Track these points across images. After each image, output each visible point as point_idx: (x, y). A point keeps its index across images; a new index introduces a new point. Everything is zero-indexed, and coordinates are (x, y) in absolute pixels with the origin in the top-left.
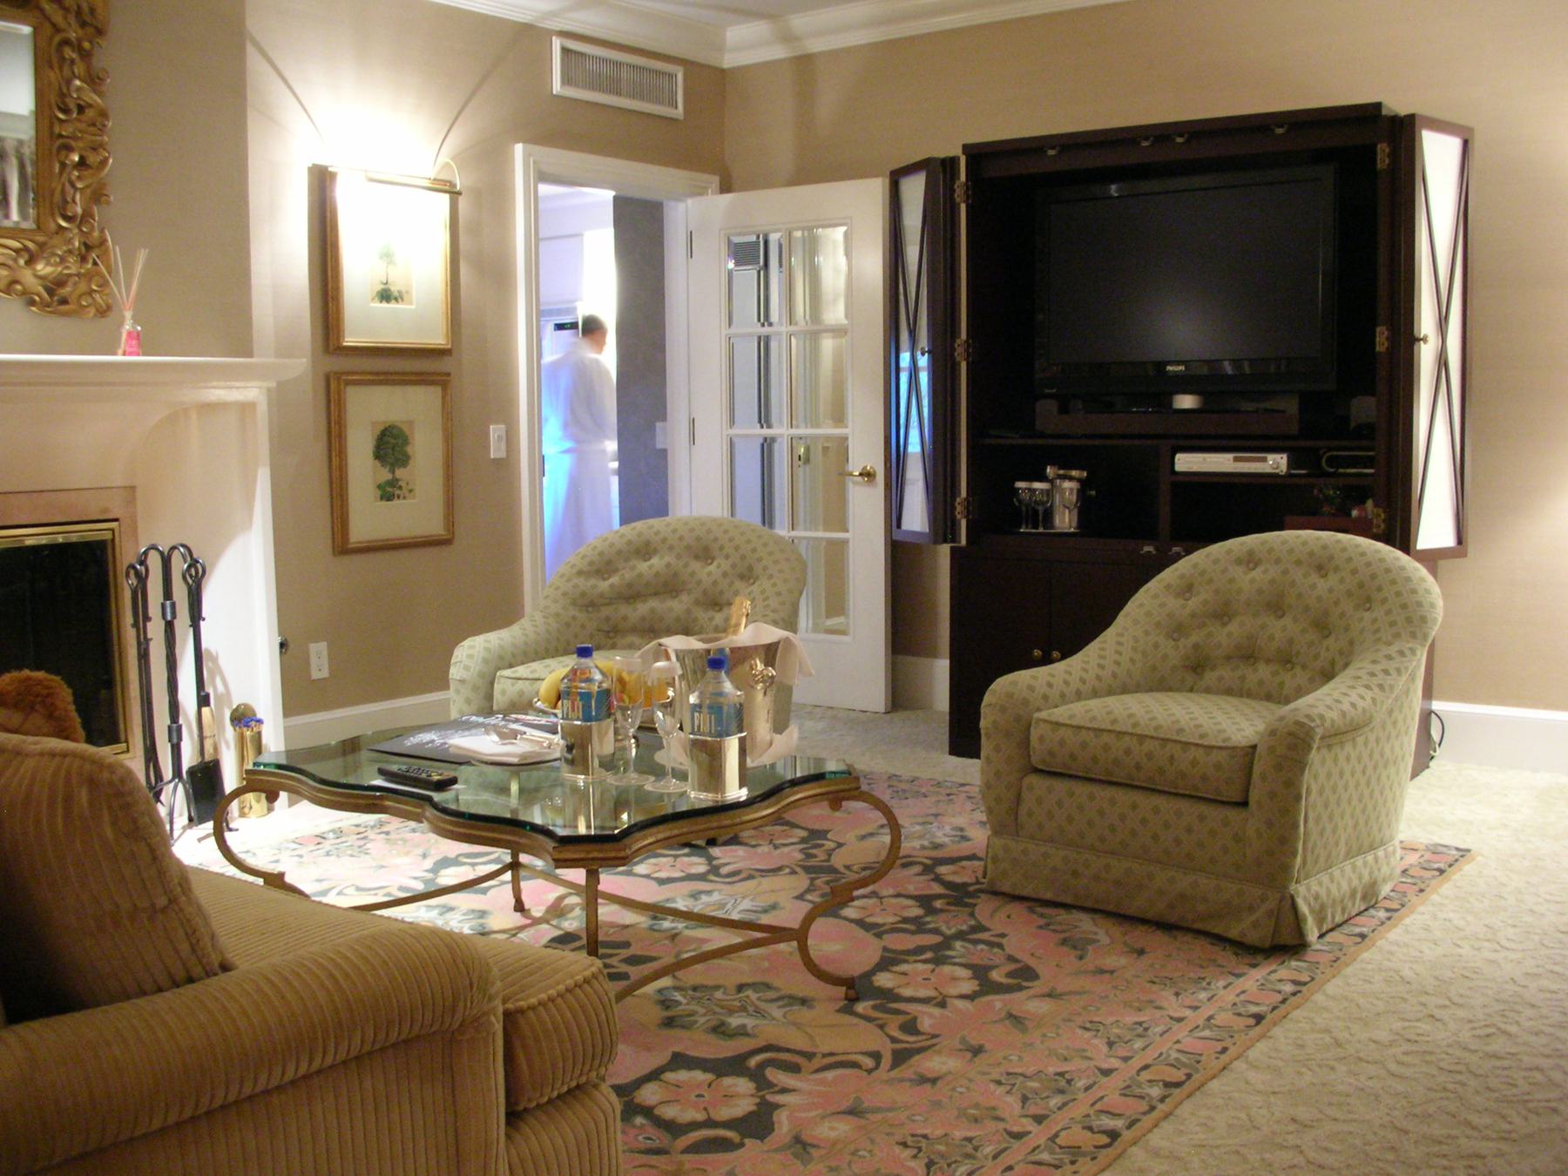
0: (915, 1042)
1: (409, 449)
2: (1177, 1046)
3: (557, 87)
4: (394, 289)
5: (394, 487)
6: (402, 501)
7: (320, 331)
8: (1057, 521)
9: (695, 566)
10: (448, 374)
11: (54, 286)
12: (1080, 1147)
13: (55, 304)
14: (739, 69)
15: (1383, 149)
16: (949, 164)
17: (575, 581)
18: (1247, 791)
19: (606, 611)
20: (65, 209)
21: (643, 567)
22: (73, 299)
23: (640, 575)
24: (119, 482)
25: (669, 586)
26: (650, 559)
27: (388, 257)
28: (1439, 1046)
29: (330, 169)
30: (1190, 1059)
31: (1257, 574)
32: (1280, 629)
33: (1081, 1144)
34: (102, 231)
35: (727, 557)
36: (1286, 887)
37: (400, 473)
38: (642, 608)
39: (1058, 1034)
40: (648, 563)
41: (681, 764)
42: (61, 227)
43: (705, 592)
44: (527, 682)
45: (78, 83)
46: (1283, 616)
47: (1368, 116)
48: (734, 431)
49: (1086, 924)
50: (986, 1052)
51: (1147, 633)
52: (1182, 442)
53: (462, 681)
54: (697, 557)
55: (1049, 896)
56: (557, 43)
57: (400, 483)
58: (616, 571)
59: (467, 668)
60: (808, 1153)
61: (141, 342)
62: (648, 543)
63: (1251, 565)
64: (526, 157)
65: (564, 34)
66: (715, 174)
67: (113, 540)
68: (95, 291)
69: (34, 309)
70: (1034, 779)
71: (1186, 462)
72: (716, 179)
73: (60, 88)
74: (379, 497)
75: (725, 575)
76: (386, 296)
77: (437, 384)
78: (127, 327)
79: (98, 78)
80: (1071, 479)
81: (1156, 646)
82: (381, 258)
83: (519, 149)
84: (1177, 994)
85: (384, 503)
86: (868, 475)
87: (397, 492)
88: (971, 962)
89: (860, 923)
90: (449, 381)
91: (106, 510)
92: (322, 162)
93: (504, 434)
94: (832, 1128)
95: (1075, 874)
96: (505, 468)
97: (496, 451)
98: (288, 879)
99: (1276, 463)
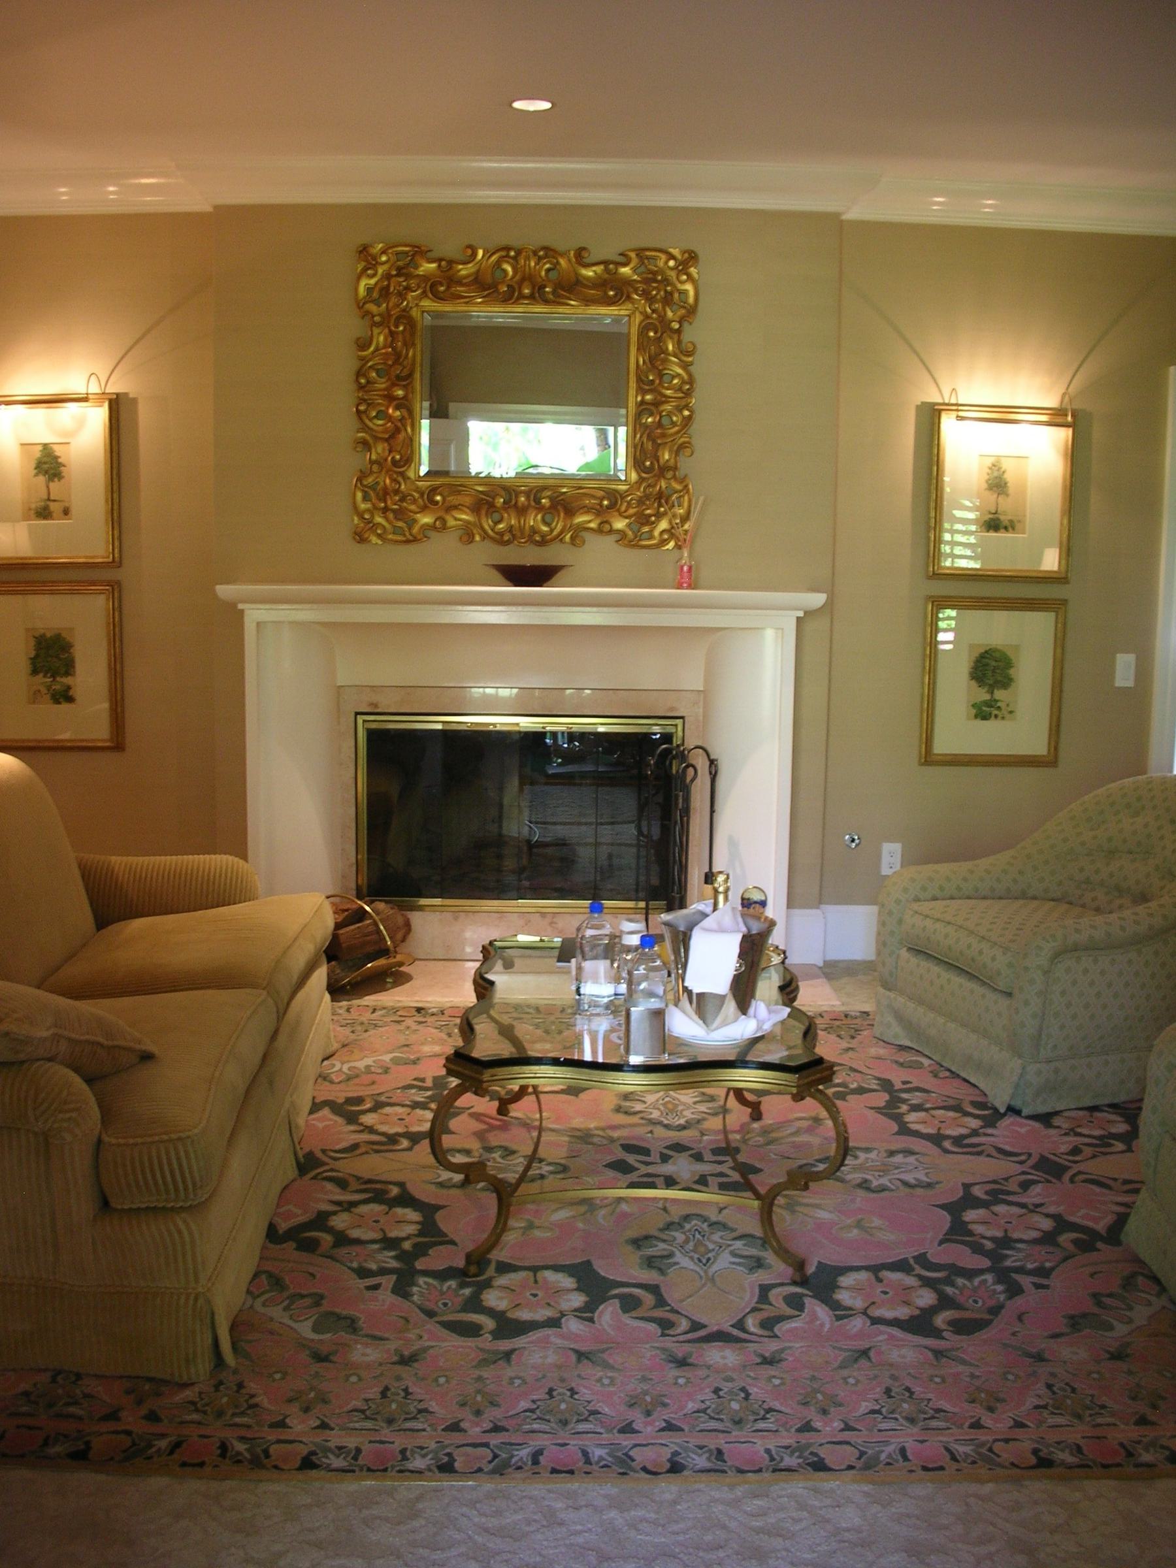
87: (995, 712)
91: (672, 709)
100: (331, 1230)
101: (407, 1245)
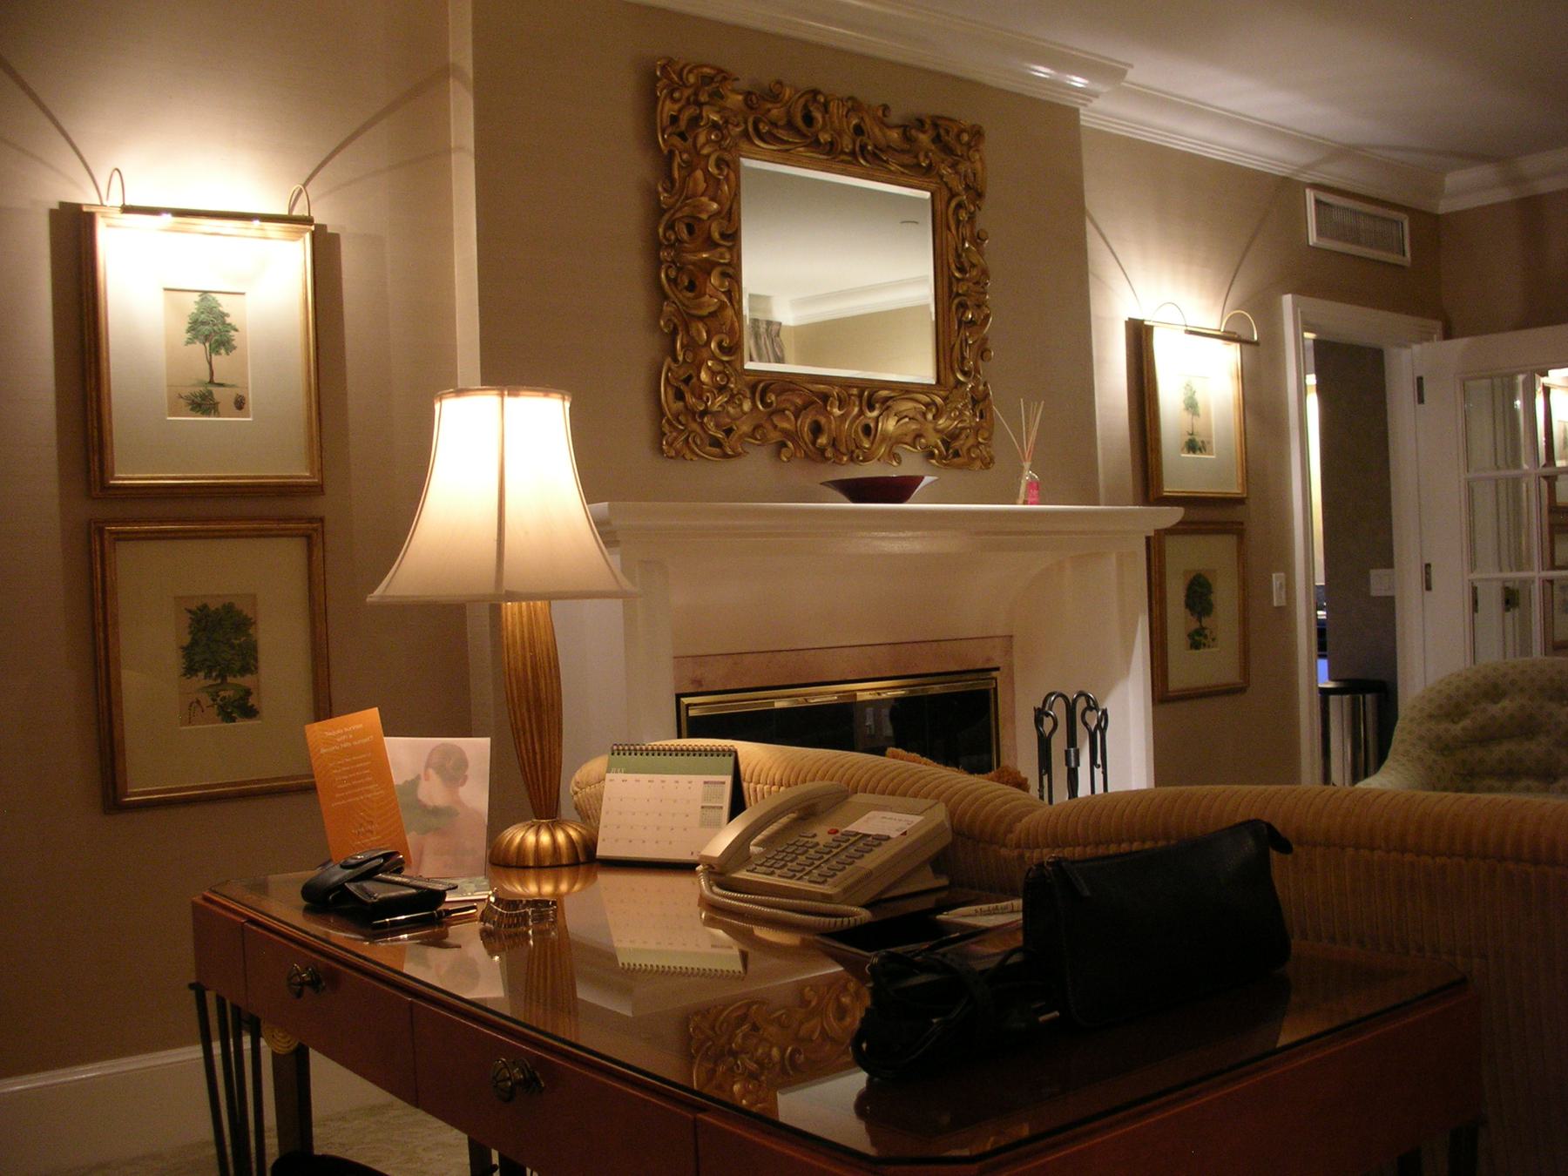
1: (1212, 597)
3: (1313, 238)
4: (1198, 439)
5: (1201, 635)
6: (1207, 650)
10: (1242, 523)
11: (950, 438)
14: (1458, 214)
20: (962, 363)
21: (1495, 709)
22: (963, 451)
24: (999, 632)
25: (1526, 727)
29: (1146, 323)
34: (985, 385)
37: (1206, 621)
38: (1499, 751)
40: (1499, 706)
42: (958, 381)
48: (1476, 576)
54: (1551, 699)
56: (1310, 195)
61: (1039, 491)
62: (1495, 686)
65: (1316, 186)
69: (934, 461)
72: (1438, 325)
76: (1192, 446)
83: (1287, 299)
85: (1194, 651)
91: (988, 660)
92: (1138, 316)
93: (1284, 583)
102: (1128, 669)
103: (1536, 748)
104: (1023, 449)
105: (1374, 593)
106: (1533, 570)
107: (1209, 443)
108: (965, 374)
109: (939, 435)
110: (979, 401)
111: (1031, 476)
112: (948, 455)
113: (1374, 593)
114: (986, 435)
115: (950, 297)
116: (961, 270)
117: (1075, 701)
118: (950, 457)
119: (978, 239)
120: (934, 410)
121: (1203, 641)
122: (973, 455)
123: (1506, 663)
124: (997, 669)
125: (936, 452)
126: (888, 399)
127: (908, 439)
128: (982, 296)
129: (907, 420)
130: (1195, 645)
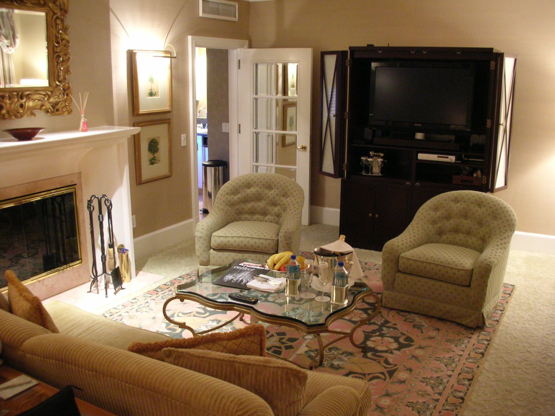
0: (391, 368)
1: (158, 146)
2: (465, 365)
3: (201, 14)
4: (153, 91)
7: (131, 109)
8: (374, 170)
9: (266, 191)
10: (170, 119)
11: (55, 105)
12: (455, 404)
13: (55, 112)
15: (493, 64)
16: (344, 53)
17: (226, 197)
18: (470, 283)
19: (237, 207)
20: (58, 78)
22: (60, 109)
23: (248, 194)
25: (258, 198)
26: (250, 188)
27: (151, 80)
28: (533, 362)
30: (471, 370)
31: (458, 205)
32: (466, 223)
33: (455, 402)
34: (68, 84)
35: (277, 189)
36: (481, 310)
37: (156, 155)
38: (250, 205)
39: (430, 363)
41: (320, 288)
42: (57, 85)
43: (270, 200)
44: (224, 238)
45: (61, 31)
46: (467, 219)
47: (489, 51)
49: (418, 319)
50: (413, 370)
51: (425, 223)
52: (420, 150)
53: (200, 237)
54: (267, 188)
55: (403, 309)
57: (156, 158)
58: (239, 193)
59: (202, 233)
60: (383, 411)
62: (249, 183)
63: (456, 202)
64: (192, 40)
66: (246, 40)
67: (75, 192)
68: (68, 106)
69: (48, 114)
70: (399, 274)
71: (422, 156)
72: (247, 42)
73: (56, 35)
74: (150, 164)
75: (277, 195)
76: (151, 94)
77: (165, 123)
78: (82, 120)
79: (66, 29)
80: (379, 157)
81: (428, 227)
82: (150, 81)
83: (190, 38)
84: (456, 346)
86: (304, 148)
87: (155, 161)
88: (393, 335)
89: (350, 320)
90: (170, 122)
91: (72, 182)
94: (385, 401)
95: (413, 303)
96: (186, 149)
97: (183, 144)
98: (186, 325)
99: (452, 159)
100: (399, 343)
101: (378, 334)
102: (122, 184)
103: (261, 205)
104: (81, 111)
105: (223, 131)
106: (273, 130)
107: (157, 92)
108: (59, 82)
109: (51, 104)
110: (66, 91)
111: (85, 120)
112: (54, 111)
113: (223, 131)
114: (69, 102)
115: (53, 53)
116: (58, 43)
117: (101, 198)
118: (55, 112)
119: (65, 29)
120: (47, 97)
121: (155, 161)
122: (64, 110)
123: (253, 175)
124: (76, 184)
125: (50, 110)
126: (28, 95)
127: (38, 107)
128: (67, 51)
129: (37, 101)
130: (152, 163)
